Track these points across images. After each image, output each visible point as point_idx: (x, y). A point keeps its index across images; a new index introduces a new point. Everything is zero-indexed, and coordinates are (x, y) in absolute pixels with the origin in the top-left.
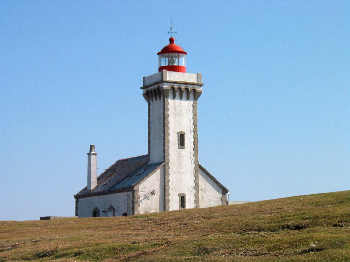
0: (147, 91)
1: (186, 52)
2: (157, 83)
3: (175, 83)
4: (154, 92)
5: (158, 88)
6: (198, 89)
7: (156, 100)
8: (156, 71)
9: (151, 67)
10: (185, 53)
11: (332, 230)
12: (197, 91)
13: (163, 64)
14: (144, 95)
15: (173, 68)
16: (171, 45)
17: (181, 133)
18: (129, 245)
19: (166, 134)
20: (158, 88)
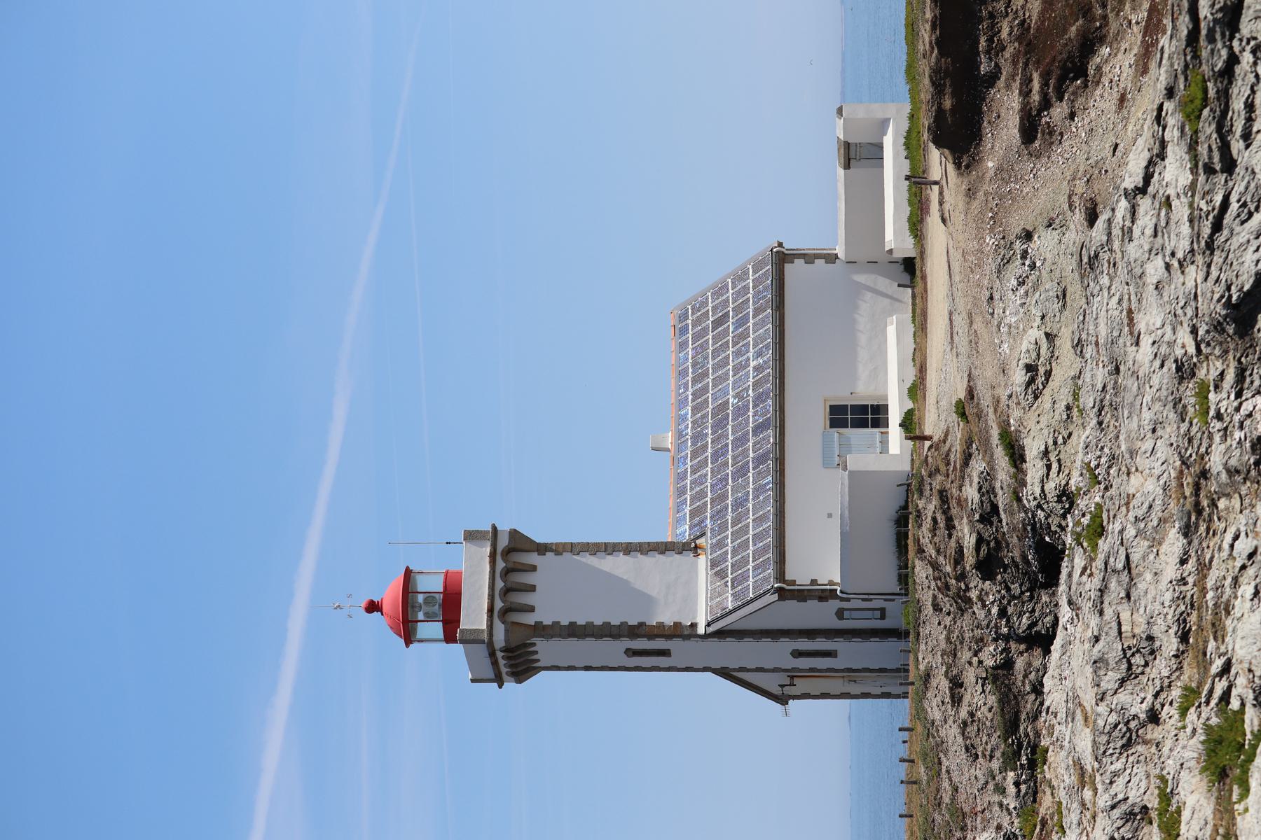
2: (492, 654)
3: (491, 610)
4: (513, 659)
5: (505, 650)
6: (503, 542)
7: (536, 652)
8: (458, 649)
9: (441, 663)
10: (408, 573)
11: (941, 559)
13: (436, 629)
14: (520, 681)
15: (450, 602)
18: (940, 763)
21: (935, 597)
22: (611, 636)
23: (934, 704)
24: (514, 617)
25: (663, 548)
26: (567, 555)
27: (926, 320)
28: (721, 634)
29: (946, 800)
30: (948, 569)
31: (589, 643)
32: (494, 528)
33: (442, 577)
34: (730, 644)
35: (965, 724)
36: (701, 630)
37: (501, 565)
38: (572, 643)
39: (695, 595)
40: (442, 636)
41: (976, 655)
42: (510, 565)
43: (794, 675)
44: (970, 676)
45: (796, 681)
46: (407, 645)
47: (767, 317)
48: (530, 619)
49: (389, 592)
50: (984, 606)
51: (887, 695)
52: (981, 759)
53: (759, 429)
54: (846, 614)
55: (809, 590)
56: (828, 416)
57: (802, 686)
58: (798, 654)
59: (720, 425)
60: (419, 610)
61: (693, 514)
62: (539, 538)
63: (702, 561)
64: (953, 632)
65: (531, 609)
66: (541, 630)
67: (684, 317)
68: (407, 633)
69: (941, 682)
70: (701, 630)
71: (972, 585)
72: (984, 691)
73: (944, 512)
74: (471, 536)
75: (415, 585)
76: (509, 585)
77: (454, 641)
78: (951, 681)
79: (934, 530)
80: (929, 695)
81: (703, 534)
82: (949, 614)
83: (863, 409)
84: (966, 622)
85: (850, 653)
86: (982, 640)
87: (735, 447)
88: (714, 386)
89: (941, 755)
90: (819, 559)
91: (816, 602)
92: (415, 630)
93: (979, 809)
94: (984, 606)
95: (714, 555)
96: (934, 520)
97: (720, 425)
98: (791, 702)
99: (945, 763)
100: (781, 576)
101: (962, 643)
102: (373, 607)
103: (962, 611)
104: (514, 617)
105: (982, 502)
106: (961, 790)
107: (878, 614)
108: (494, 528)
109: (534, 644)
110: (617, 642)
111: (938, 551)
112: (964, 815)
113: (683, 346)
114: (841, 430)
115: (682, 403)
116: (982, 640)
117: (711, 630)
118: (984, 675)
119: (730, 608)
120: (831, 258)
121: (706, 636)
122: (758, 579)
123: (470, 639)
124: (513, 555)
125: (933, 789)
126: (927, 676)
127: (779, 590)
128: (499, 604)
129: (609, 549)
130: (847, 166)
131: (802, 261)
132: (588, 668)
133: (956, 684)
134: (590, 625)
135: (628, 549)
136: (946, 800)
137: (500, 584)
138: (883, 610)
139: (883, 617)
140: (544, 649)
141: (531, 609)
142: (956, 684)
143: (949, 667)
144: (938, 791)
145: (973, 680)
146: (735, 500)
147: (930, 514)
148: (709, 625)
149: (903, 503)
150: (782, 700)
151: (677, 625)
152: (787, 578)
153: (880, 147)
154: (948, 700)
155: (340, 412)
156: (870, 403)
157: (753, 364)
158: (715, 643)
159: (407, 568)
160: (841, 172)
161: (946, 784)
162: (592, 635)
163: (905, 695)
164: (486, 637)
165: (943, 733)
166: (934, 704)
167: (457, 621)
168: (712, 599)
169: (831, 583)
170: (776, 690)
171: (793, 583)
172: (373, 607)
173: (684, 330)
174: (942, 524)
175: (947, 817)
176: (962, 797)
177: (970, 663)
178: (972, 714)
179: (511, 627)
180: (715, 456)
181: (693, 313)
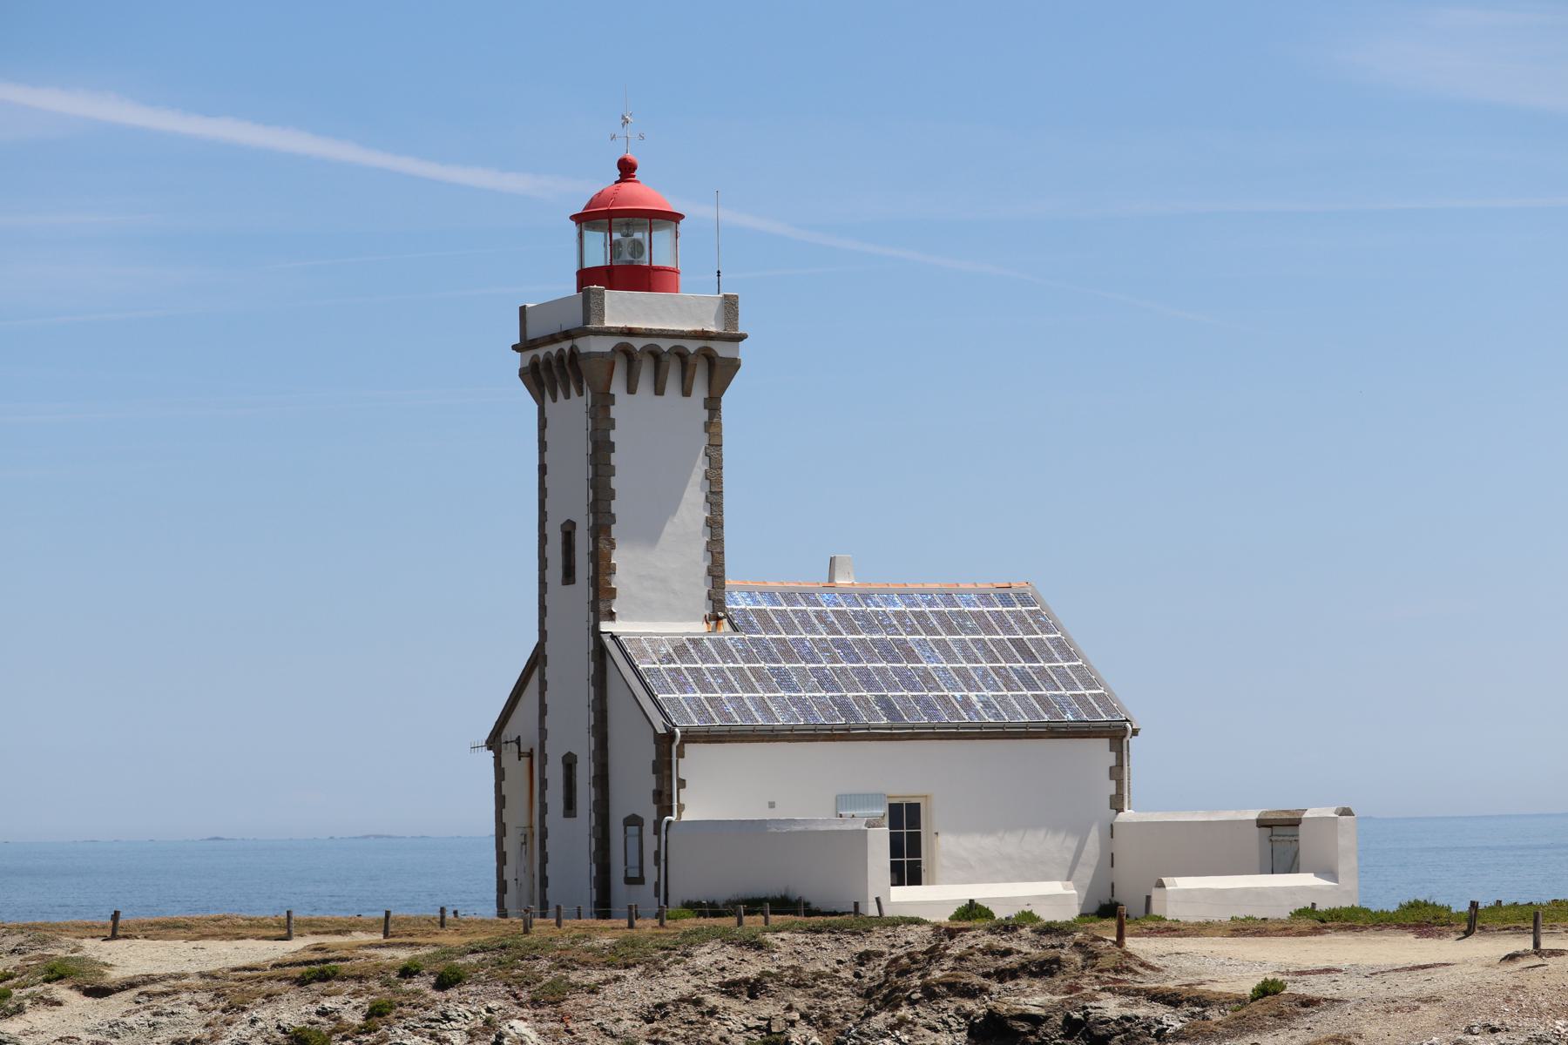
1: (675, 208)
2: (568, 335)
3: (630, 332)
4: (559, 364)
6: (722, 350)
7: (567, 396)
8: (568, 287)
10: (676, 217)
14: (523, 374)
15: (642, 278)
16: (627, 187)
18: (627, 967)
21: (880, 955)
22: (595, 500)
23: (718, 957)
24: (610, 367)
25: (716, 573)
26: (704, 439)
27: (1254, 934)
28: (600, 653)
29: (574, 977)
30: (937, 974)
31: (583, 471)
32: (742, 337)
33: (671, 265)
34: (586, 667)
35: (698, 1003)
36: (605, 626)
37: (692, 346)
38: (583, 447)
39: (653, 618)
40: (587, 265)
41: (803, 1016)
42: (691, 360)
43: (534, 757)
44: (767, 1008)
45: (525, 760)
46: (574, 217)
47: (1038, 716)
48: (618, 387)
49: (649, 190)
50: (893, 1027)
51: (502, 887)
52: (647, 1027)
53: (886, 703)
54: (633, 830)
55: (671, 776)
56: (905, 801)
57: (516, 768)
58: (569, 763)
59: (887, 651)
60: (623, 234)
61: (761, 614)
62: (727, 400)
63: (699, 628)
64: (831, 982)
65: (631, 390)
66: (602, 402)
67: (1025, 600)
68: (591, 218)
69: (753, 967)
70: (605, 626)
71: (919, 1009)
72: (749, 1029)
73: (1023, 967)
74: (730, 306)
75: (660, 228)
76: (664, 358)
77: (581, 285)
78: (757, 980)
79: (990, 951)
80: (730, 949)
81: (735, 629)
82: (857, 975)
83: (915, 849)
84: (849, 1001)
85: (571, 839)
86: (827, 1025)
87: (859, 672)
88: (936, 642)
89: (641, 969)
90: (713, 791)
91: (654, 787)
92: (594, 229)
93: (572, 1026)
94: (893, 1027)
95: (707, 643)
96: (1007, 953)
97: (887, 651)
98: (491, 753)
99: (631, 974)
100: (691, 737)
101: (817, 995)
102: (627, 169)
103: (868, 995)
104: (610, 367)
105: (1107, 1022)
106: (594, 999)
107: (634, 873)
108: (742, 337)
109: (580, 393)
110: (585, 509)
111: (960, 958)
112: (556, 1003)
113: (985, 598)
114: (886, 821)
115: (905, 595)
116: (827, 1025)
117: (607, 640)
118: (774, 1030)
119: (641, 667)
120: (1117, 803)
121: (597, 634)
122: (685, 704)
123: (590, 306)
124: (704, 364)
125: (584, 957)
126: (759, 946)
127: (671, 736)
128: (638, 344)
129: (714, 498)
130: (1262, 823)
131: (1113, 763)
132: (543, 469)
133: (754, 989)
134: (611, 471)
135: (714, 524)
136: (574, 977)
137: (665, 345)
138: (640, 880)
139: (629, 881)
140: (573, 409)
141: (631, 390)
142: (754, 989)
143: (777, 978)
144: (584, 964)
145: (764, 1014)
146: (786, 672)
147: (1014, 945)
148: (614, 637)
149: (814, 906)
150: (494, 741)
151: (612, 593)
152: (688, 747)
153: (1292, 867)
154: (728, 977)
155: (513, 182)
156: (923, 859)
157: (973, 695)
158: (586, 645)
159: (681, 216)
160: (1253, 815)
161: (596, 976)
162: (596, 474)
163: (502, 913)
164: (593, 325)
165: (677, 970)
166: (718, 957)
167: (612, 286)
168: (651, 641)
169: (681, 808)
170: (509, 733)
171: (681, 755)
172: (627, 169)
173: (1006, 601)
174: (1003, 963)
175: (547, 979)
176: (583, 999)
177: (790, 1008)
178: (712, 1012)
179: (608, 361)
180: (842, 645)
181: (1030, 612)
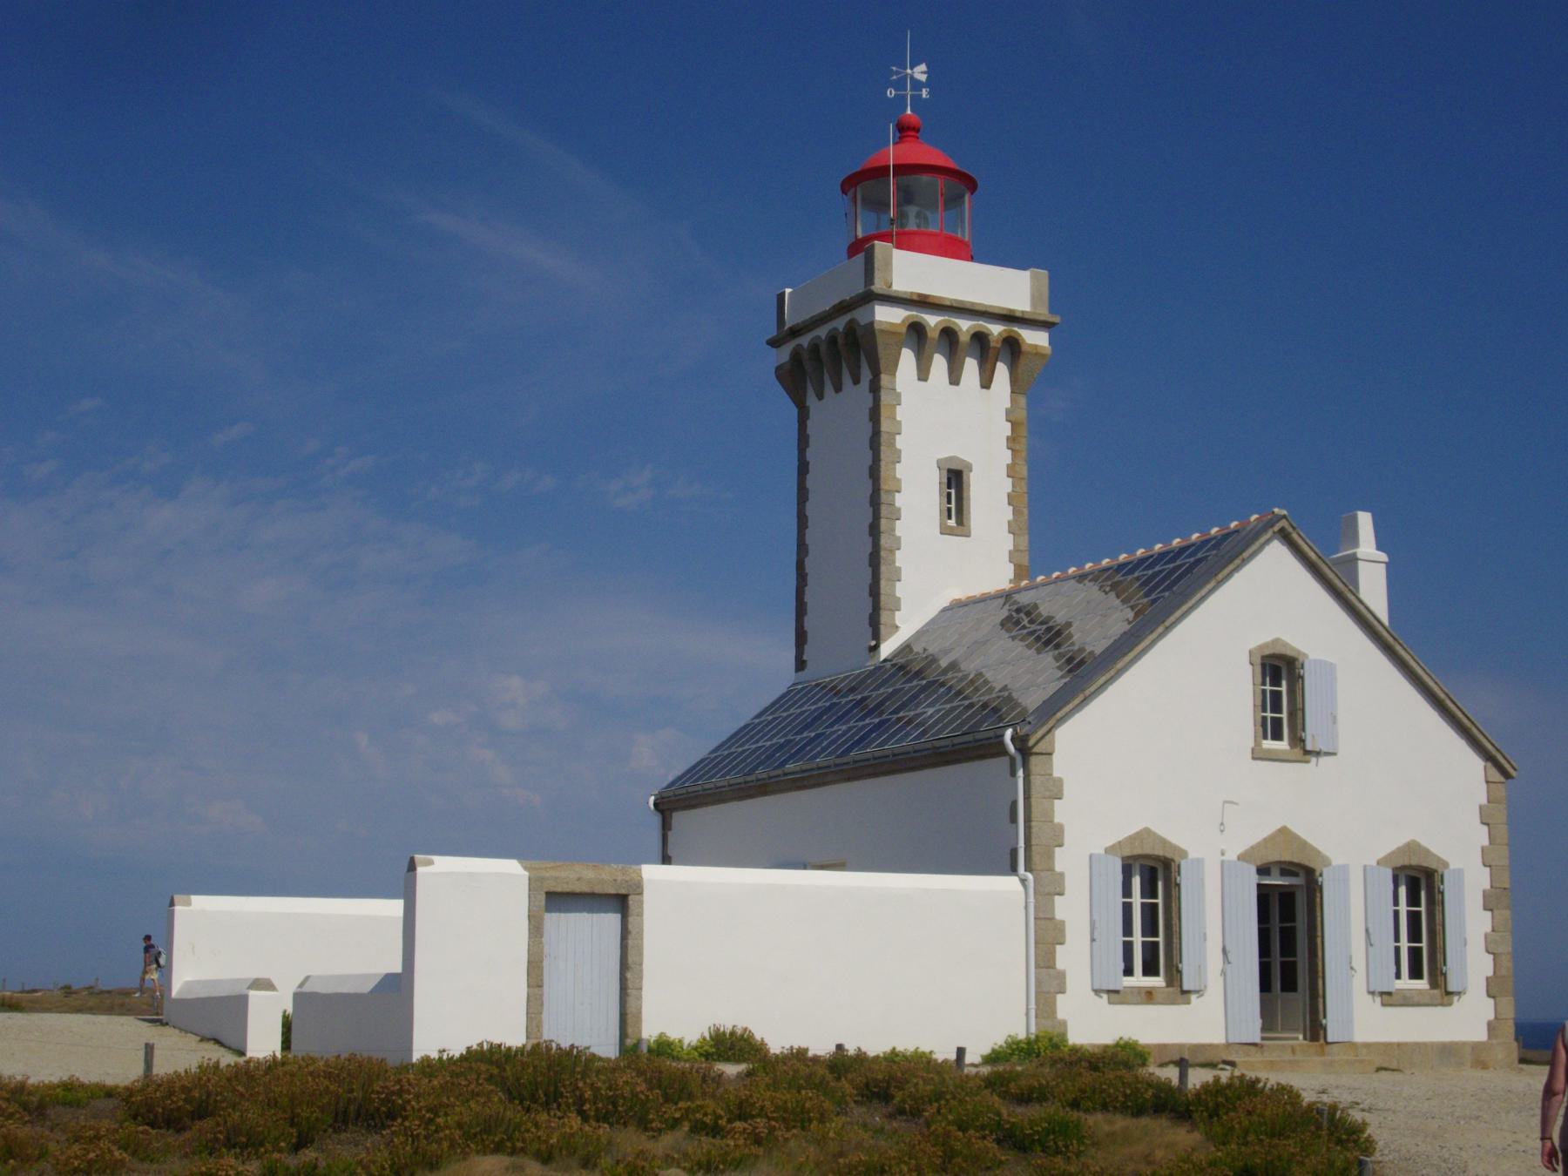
0: (796, 356)
2: (842, 308)
5: (851, 328)
12: (1024, 348)
17: (954, 466)
19: (884, 510)
20: (851, 328)
